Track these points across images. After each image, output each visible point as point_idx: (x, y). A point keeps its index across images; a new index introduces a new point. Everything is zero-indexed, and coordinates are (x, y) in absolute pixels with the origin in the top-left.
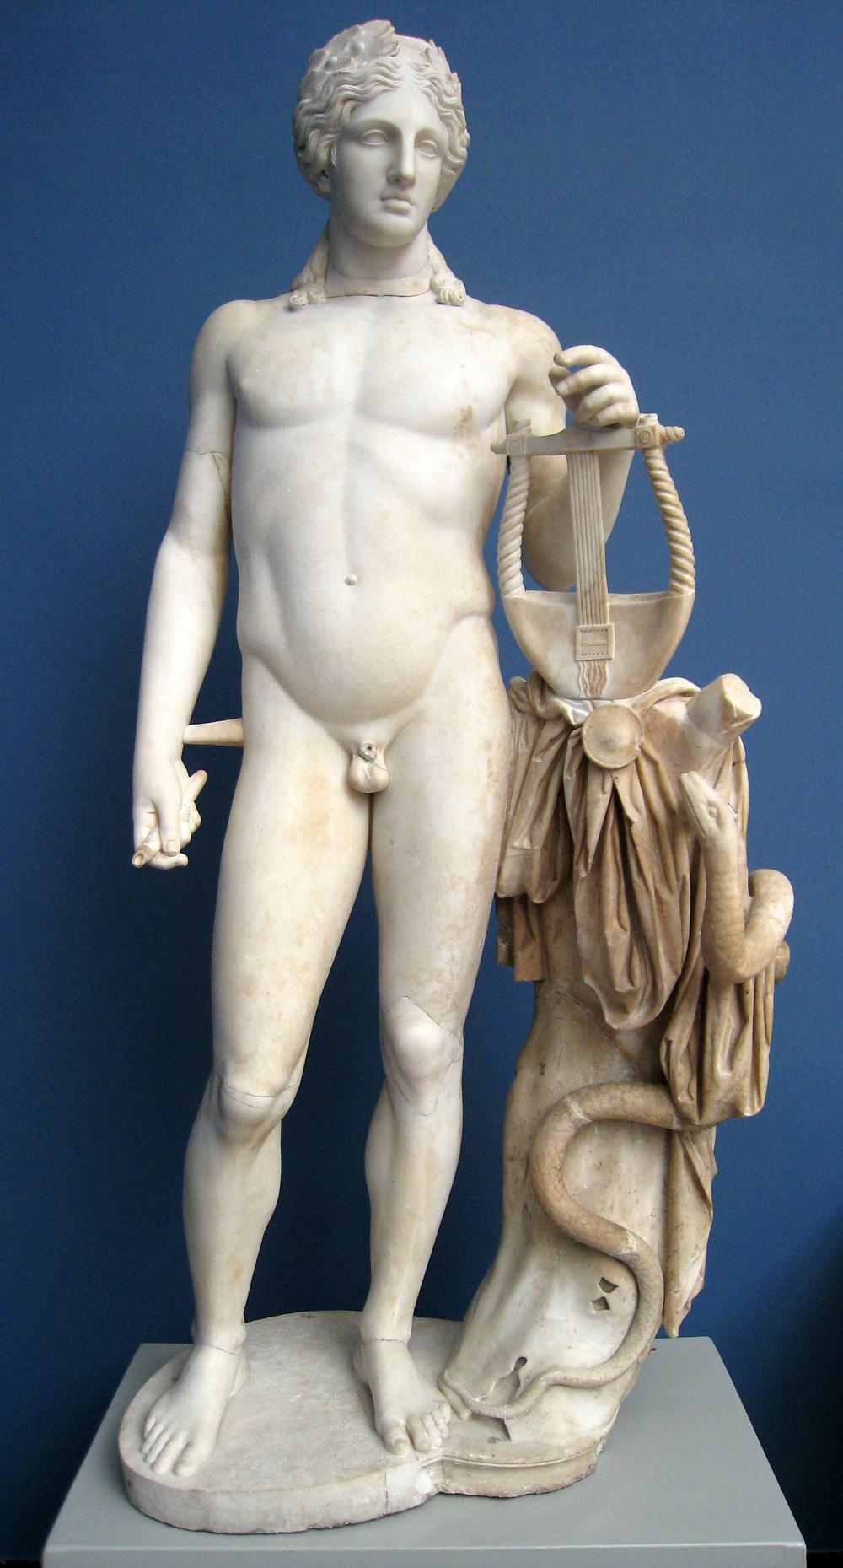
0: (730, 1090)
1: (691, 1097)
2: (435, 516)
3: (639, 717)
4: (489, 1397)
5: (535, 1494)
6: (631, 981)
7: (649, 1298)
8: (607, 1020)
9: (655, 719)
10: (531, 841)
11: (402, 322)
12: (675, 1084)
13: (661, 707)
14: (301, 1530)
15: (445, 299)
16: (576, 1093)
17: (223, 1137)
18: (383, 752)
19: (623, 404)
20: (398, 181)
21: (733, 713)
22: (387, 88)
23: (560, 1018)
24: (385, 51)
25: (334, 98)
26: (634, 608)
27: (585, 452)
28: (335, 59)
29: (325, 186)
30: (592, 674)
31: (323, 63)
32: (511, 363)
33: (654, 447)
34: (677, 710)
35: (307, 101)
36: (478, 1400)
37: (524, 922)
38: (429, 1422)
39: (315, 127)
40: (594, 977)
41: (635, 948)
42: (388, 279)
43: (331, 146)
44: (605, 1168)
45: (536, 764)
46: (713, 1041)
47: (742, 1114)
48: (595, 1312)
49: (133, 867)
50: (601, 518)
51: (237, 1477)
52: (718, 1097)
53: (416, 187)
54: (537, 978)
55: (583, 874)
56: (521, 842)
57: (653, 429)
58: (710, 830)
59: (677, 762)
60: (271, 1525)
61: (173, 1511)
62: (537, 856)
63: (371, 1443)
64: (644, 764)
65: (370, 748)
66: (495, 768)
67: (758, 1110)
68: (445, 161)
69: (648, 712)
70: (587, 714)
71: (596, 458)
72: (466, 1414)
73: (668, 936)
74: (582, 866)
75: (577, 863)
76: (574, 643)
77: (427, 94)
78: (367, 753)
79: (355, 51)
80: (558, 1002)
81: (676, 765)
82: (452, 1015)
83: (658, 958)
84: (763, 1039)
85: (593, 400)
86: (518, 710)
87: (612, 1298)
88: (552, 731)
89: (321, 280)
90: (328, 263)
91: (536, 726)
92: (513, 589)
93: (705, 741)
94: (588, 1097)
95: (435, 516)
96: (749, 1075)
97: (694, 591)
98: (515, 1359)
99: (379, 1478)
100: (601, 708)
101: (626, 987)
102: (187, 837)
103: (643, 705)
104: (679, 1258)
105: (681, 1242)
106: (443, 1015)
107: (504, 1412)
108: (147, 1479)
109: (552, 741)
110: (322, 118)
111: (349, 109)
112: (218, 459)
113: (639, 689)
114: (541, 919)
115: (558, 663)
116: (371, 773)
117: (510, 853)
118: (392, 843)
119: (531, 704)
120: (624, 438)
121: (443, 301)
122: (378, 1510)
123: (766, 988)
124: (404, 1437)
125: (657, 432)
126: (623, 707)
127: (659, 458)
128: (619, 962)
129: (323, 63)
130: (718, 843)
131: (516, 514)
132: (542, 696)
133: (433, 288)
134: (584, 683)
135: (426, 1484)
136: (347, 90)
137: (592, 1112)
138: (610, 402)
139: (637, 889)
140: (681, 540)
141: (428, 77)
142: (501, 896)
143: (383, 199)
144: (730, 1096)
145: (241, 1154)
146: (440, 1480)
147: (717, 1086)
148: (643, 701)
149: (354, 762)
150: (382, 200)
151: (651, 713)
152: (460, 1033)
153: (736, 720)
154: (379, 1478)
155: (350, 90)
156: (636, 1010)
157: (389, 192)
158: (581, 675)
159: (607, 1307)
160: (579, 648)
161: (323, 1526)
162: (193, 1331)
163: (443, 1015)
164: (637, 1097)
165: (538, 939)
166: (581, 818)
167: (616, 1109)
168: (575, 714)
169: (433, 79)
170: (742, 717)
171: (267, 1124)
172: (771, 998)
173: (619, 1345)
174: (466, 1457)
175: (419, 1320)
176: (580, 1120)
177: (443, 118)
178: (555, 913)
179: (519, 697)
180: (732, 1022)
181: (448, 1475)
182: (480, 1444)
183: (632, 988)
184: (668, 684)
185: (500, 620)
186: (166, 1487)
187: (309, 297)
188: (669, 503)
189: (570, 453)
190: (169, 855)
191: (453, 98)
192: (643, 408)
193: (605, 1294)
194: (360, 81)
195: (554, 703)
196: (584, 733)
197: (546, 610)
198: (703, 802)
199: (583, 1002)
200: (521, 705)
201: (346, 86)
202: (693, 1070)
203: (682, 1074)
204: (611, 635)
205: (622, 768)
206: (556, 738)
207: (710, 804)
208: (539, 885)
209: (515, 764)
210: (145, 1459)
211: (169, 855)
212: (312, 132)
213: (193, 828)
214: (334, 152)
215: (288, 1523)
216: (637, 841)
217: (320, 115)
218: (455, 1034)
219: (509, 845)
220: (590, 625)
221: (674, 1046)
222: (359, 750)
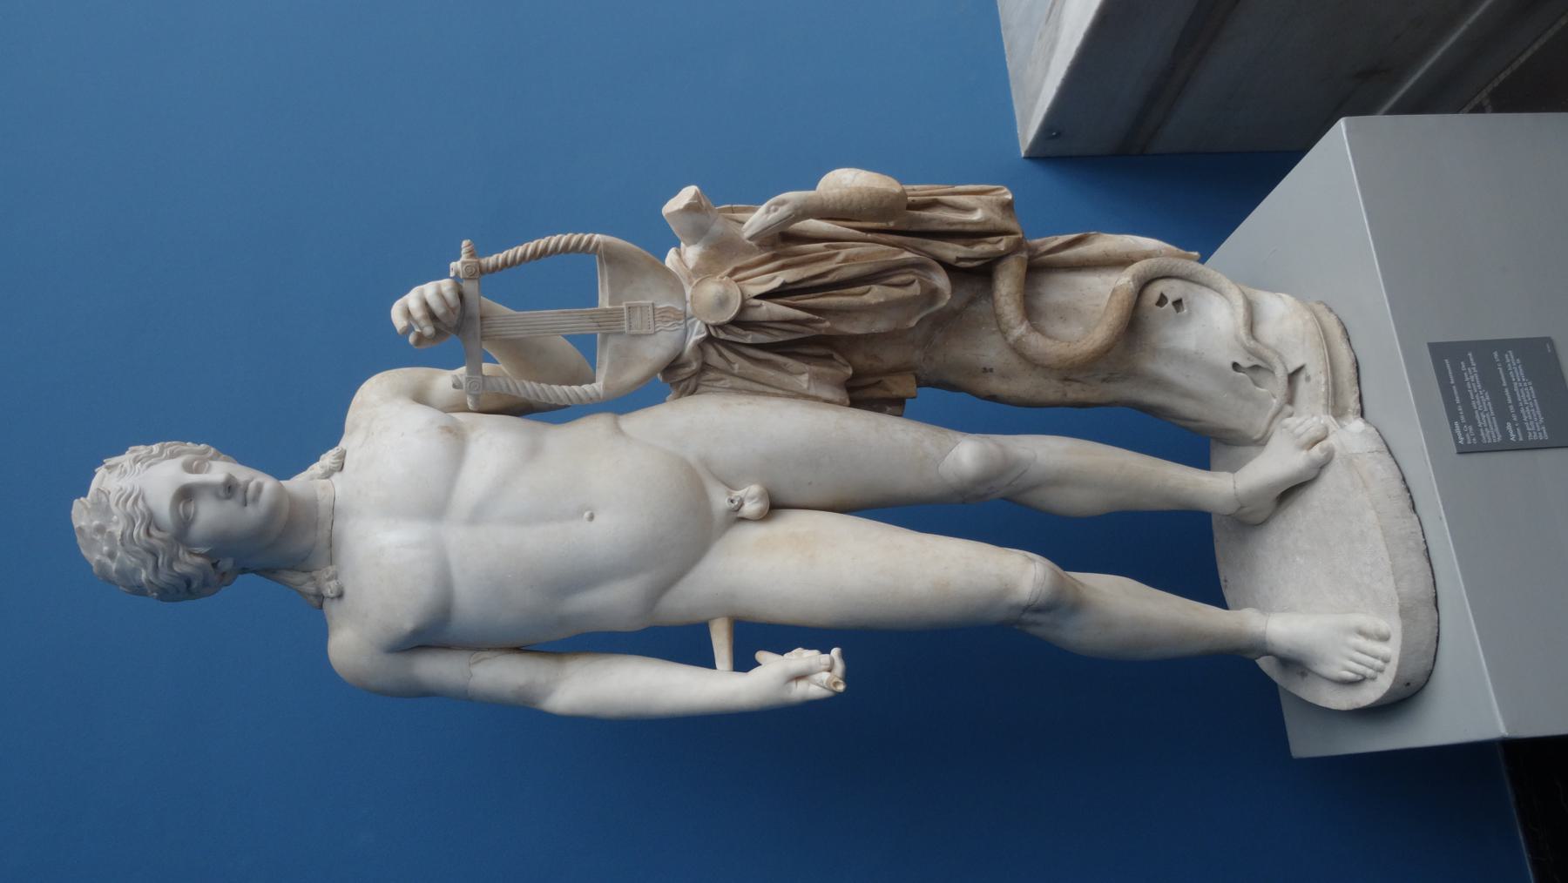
0: (992, 210)
1: (1001, 240)
2: (533, 452)
4: (1274, 389)
5: (1349, 340)
6: (912, 283)
7: (1168, 267)
10: (804, 373)
14: (1417, 519)
20: (229, 488)
22: (141, 496)
24: (104, 499)
27: (482, 325)
28: (105, 548)
29: (227, 564)
30: (665, 319)
33: (479, 264)
35: (144, 575)
38: (1300, 430)
39: (170, 566)
43: (191, 553)
45: (739, 369)
46: (954, 224)
48: (1185, 311)
49: (846, 690)
52: (999, 220)
54: (913, 378)
55: (828, 324)
57: (463, 263)
62: (815, 369)
63: (1328, 477)
64: (737, 276)
65: (732, 501)
67: (1006, 190)
70: (698, 323)
72: (1289, 409)
74: (821, 325)
75: (820, 330)
76: (639, 336)
77: (149, 466)
78: (736, 503)
79: (100, 529)
81: (736, 255)
84: (950, 189)
87: (1171, 298)
88: (713, 357)
90: (297, 570)
93: (717, 228)
98: (1234, 373)
99: (1358, 458)
100: (693, 309)
102: (815, 652)
103: (689, 277)
105: (1119, 251)
107: (1281, 374)
109: (721, 355)
110: (163, 558)
111: (157, 531)
115: (656, 350)
116: (753, 498)
117: (813, 392)
118: (810, 483)
122: (1386, 457)
124: (1317, 448)
128: (897, 293)
129: (108, 561)
131: (532, 386)
132: (684, 365)
133: (328, 474)
142: (848, 402)
144: (997, 210)
146: (1351, 417)
147: (989, 220)
148: (687, 278)
150: (246, 505)
153: (700, 202)
154: (1358, 458)
157: (239, 496)
160: (644, 331)
165: (883, 378)
167: (1015, 300)
170: (696, 196)
175: (1212, 465)
182: (1313, 388)
183: (917, 281)
185: (622, 403)
187: (329, 579)
188: (526, 250)
189: (482, 337)
190: (832, 662)
192: (444, 274)
193: (1170, 302)
194: (131, 521)
196: (713, 322)
200: (691, 388)
201: (135, 533)
207: (768, 211)
210: (1381, 671)
211: (832, 662)
212: (176, 569)
215: (1414, 530)
216: (798, 277)
217: (160, 561)
221: (961, 255)
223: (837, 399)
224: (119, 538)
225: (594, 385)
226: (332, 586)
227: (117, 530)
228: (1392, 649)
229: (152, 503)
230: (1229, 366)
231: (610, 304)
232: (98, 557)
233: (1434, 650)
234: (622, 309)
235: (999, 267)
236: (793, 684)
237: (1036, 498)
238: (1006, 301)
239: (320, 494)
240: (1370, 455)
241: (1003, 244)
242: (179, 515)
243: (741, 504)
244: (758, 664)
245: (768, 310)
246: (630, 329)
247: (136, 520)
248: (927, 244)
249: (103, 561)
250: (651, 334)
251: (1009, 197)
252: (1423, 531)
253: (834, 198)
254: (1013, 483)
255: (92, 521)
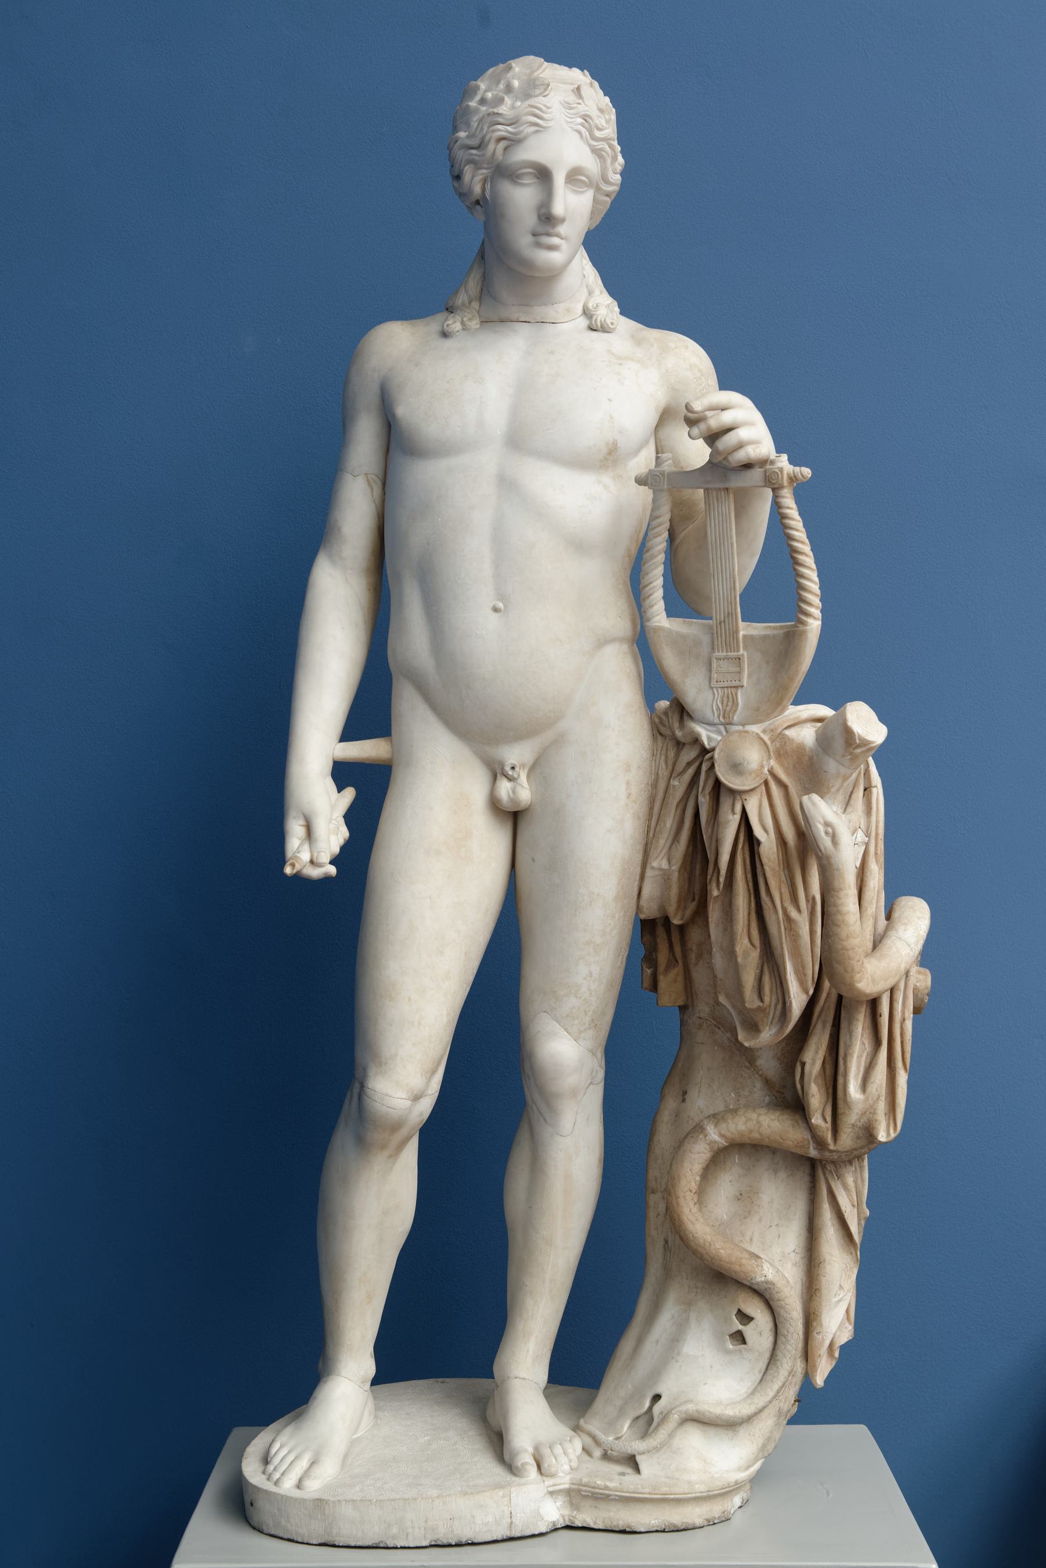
0: (864, 1114)
1: (826, 1122)
2: (579, 546)
3: (768, 742)
5: (664, 1531)
8: (740, 1038)
9: (785, 744)
10: (669, 861)
11: (552, 352)
12: (808, 1105)
13: (789, 733)
15: (597, 326)
16: (715, 1118)
17: (362, 1143)
18: (526, 771)
19: (753, 446)
20: (547, 219)
21: (855, 739)
22: (539, 129)
23: (702, 1043)
24: (537, 92)
25: (487, 137)
26: (765, 638)
28: (489, 95)
30: (725, 699)
31: (478, 97)
32: (660, 393)
34: (807, 735)
35: (462, 134)
36: (611, 1439)
37: (667, 945)
38: (558, 1450)
39: (470, 162)
40: (728, 996)
41: (765, 965)
42: (540, 305)
43: (485, 181)
44: (746, 1199)
45: (674, 786)
47: (877, 1139)
48: (731, 1347)
49: (285, 875)
50: (736, 556)
51: (361, 1491)
52: (852, 1119)
53: (565, 223)
54: (681, 1003)
55: (715, 893)
56: (660, 862)
58: (825, 849)
59: (807, 786)
60: (394, 1537)
61: (299, 1525)
62: (675, 876)
65: (513, 768)
66: (634, 790)
67: (893, 1135)
68: (598, 189)
69: (778, 737)
70: (719, 738)
71: (731, 495)
72: (598, 1453)
73: (797, 954)
74: (714, 885)
77: (579, 132)
78: (510, 773)
79: (509, 89)
80: (700, 1027)
82: (590, 1033)
83: (785, 973)
85: (729, 439)
86: (661, 734)
87: (748, 1331)
89: (475, 305)
91: (675, 750)
92: (654, 617)
93: (831, 766)
94: (724, 1119)
95: (579, 546)
96: (883, 1098)
97: (820, 622)
99: (503, 1497)
101: (757, 1003)
102: (336, 850)
103: (772, 730)
104: (820, 1297)
105: (823, 1280)
106: (580, 1032)
107: (636, 1446)
108: (271, 1492)
109: (689, 764)
110: (476, 155)
112: (372, 481)
113: (768, 716)
114: (683, 942)
116: (514, 791)
117: (649, 873)
118: (533, 860)
119: (671, 729)
120: (756, 475)
121: (595, 328)
123: (903, 1013)
125: (785, 473)
126: (753, 732)
127: (786, 497)
128: (749, 979)
129: (478, 97)
130: (833, 861)
132: (681, 720)
133: (587, 313)
134: (718, 709)
135: (553, 1512)
136: (499, 130)
137: (728, 1134)
138: (740, 446)
139: (765, 906)
140: (806, 576)
141: (579, 115)
142: (642, 916)
143: (534, 235)
144: (864, 1119)
145: (378, 1161)
146: (567, 1512)
148: (772, 727)
149: (498, 783)
150: (533, 235)
151: (780, 738)
152: (600, 1053)
153: (859, 746)
154: (503, 1497)
155: (503, 131)
156: (767, 1028)
157: (540, 230)
158: (715, 702)
159: (744, 1342)
160: (715, 676)
161: (445, 1542)
162: (320, 1365)
163: (580, 1032)
164: (773, 1120)
166: (714, 839)
167: (751, 1131)
168: (709, 739)
169: (586, 118)
171: (404, 1132)
172: (909, 1025)
173: (756, 1384)
174: (593, 1485)
176: (715, 1142)
177: (596, 152)
178: (695, 935)
179: (662, 722)
180: (867, 1046)
181: (573, 1505)
183: (761, 1004)
184: (800, 711)
186: (292, 1497)
187: (463, 323)
191: (606, 131)
193: (740, 1327)
195: (691, 728)
196: (716, 756)
197: (683, 637)
198: (820, 823)
199: (723, 1027)
200: (662, 729)
201: (500, 127)
202: (828, 1094)
203: (816, 1097)
204: (744, 662)
205: (752, 790)
206: (692, 761)
207: (827, 824)
208: (678, 907)
209: (656, 788)
212: (467, 167)
213: (342, 842)
214: (488, 186)
215: (410, 1537)
216: (765, 860)
217: (474, 152)
218: (594, 1054)
219: (648, 866)
220: (725, 654)
221: (807, 1068)
222: (503, 769)
223: (643, 902)
224: (496, 110)
225: (664, 614)
226: (453, 326)
227: (504, 109)
228: (288, 1485)
229: (532, 141)
230: (658, 1391)
231: (744, 636)
232: (483, 86)
233: (281, 1535)
234: (738, 651)
235: (798, 1117)
236: (302, 822)
237: (523, 1136)
238: (751, 1119)
239: (561, 307)
240: (507, 1513)
241: (819, 1120)
242: (519, 169)
243: (510, 779)
244: (340, 789)
245: (728, 822)
246: (716, 659)
247: (512, 126)
248: (824, 1026)
249: (478, 92)
250: (710, 682)
251: (882, 1137)
252: (409, 1548)
253: (842, 904)
254: (534, 1105)
255: (519, 79)
